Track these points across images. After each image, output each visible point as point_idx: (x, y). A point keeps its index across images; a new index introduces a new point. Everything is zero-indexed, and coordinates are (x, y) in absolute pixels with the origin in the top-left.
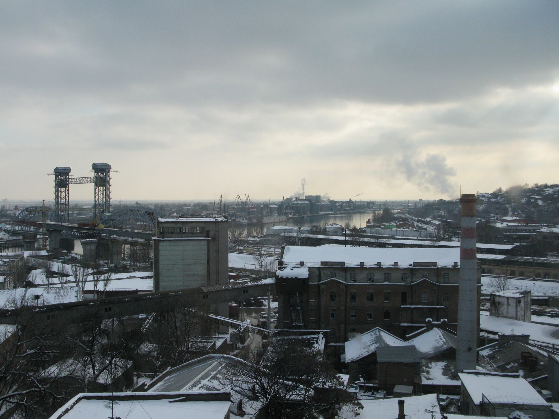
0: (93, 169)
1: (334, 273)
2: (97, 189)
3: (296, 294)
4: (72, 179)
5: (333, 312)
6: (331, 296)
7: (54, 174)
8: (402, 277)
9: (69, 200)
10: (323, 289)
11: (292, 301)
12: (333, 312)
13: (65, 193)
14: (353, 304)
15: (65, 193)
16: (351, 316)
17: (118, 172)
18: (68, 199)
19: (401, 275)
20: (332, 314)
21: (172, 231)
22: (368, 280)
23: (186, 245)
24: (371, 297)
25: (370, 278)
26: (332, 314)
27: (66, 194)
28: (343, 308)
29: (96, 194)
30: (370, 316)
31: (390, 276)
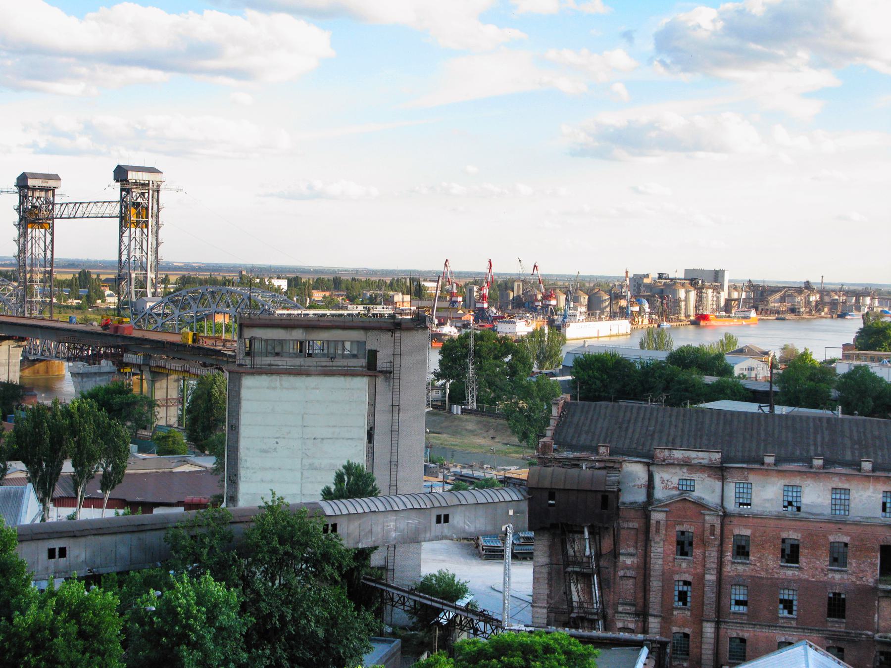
0: (118, 181)
1: (845, 489)
2: (126, 234)
3: (583, 533)
4: (62, 204)
5: (685, 588)
6: (680, 544)
7: (17, 191)
8: (884, 504)
9: (54, 260)
10: (658, 522)
11: (571, 552)
12: (685, 588)
13: (45, 243)
14: (740, 568)
15: (45, 243)
16: (733, 602)
17: (181, 190)
18: (52, 255)
19: (881, 495)
20: (680, 592)
21: (278, 350)
22: (786, 504)
23: (313, 388)
24: (791, 554)
25: (790, 499)
26: (680, 592)
27: (47, 244)
28: (711, 577)
29: (123, 247)
30: (788, 605)
31: (847, 497)
